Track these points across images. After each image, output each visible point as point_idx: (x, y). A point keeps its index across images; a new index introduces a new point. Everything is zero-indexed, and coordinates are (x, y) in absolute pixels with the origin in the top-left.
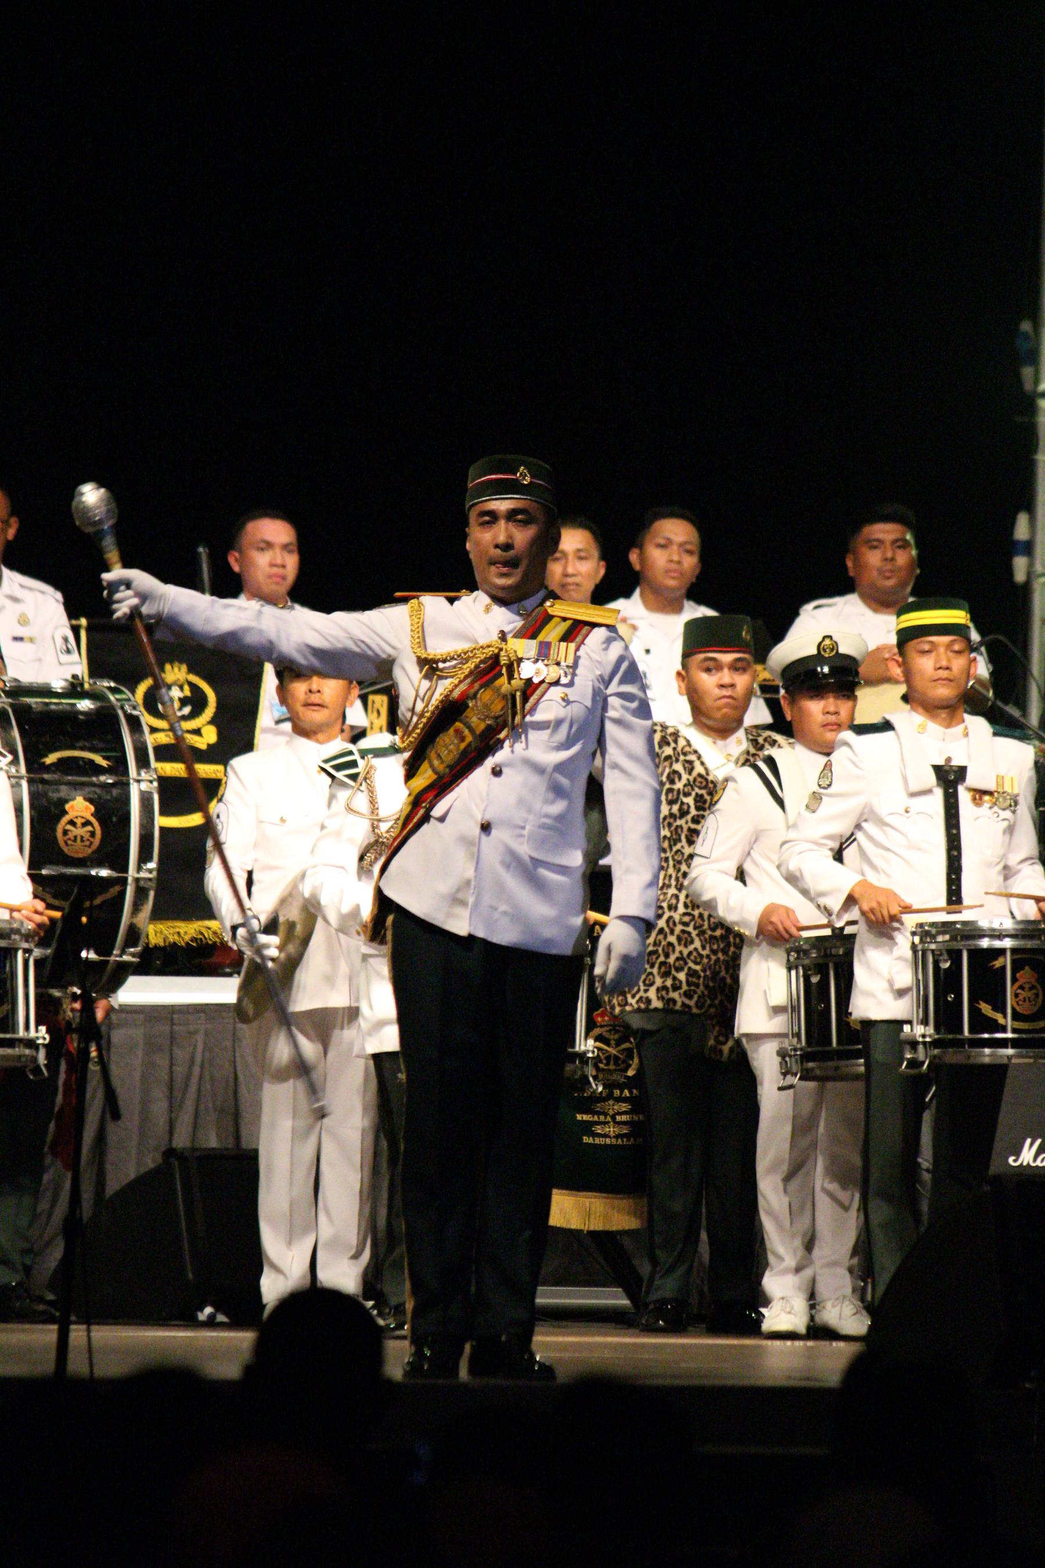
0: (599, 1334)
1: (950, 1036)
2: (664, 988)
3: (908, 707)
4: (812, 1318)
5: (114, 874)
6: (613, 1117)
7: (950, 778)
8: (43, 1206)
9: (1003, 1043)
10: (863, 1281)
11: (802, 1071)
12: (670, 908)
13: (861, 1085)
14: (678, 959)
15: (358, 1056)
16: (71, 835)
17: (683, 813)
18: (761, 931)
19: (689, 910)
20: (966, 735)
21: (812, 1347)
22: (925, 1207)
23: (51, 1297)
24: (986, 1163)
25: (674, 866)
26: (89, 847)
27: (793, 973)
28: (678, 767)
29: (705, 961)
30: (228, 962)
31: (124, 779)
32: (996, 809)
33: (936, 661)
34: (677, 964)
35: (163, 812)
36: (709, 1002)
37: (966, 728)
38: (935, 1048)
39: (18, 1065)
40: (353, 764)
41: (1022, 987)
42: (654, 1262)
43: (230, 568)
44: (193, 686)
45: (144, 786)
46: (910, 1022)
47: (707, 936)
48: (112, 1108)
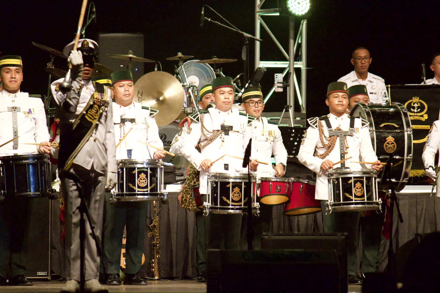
5: (400, 158)
8: (381, 250)
9: (352, 204)
16: (388, 147)
35: (414, 139)
41: (235, 193)
43: (431, 70)
44: (421, 103)
45: (409, 132)
48: (401, 220)
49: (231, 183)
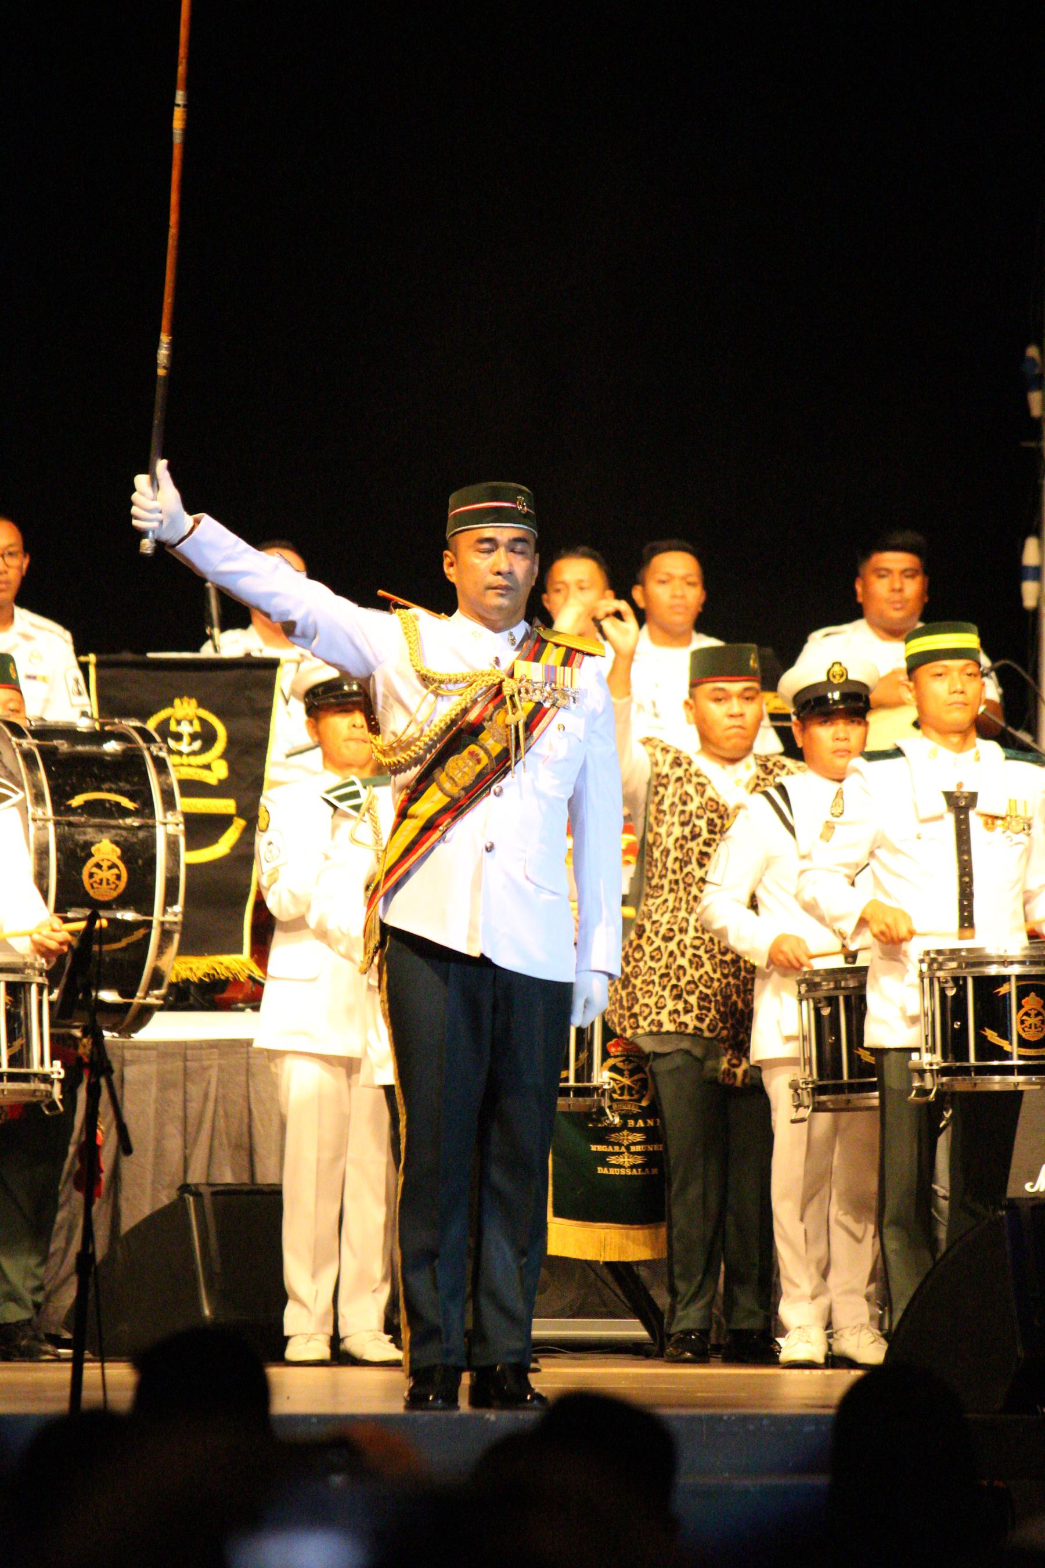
0: (616, 1366)
1: (958, 1064)
2: (676, 1011)
3: (920, 732)
4: (830, 1347)
6: (628, 1148)
7: (961, 805)
9: (1008, 1071)
10: (881, 1309)
11: (814, 1103)
12: (681, 930)
13: (878, 1113)
14: (689, 982)
15: (365, 1086)
16: (97, 878)
17: (695, 836)
18: (771, 961)
19: (699, 934)
20: (978, 759)
21: (829, 1376)
22: (942, 1234)
23: (68, 1336)
24: (1004, 1188)
25: (685, 889)
26: (115, 889)
27: (804, 1003)
28: (690, 789)
29: (716, 984)
30: (240, 996)
31: (150, 822)
32: (1009, 833)
33: (950, 686)
34: (688, 988)
36: (721, 1025)
37: (977, 753)
38: (943, 1076)
39: (35, 1100)
40: (356, 795)
41: (1027, 1014)
42: (673, 1291)
44: (203, 721)
45: (171, 829)
46: (917, 1050)
47: (717, 960)
48: (125, 1146)
49: (1013, 979)
